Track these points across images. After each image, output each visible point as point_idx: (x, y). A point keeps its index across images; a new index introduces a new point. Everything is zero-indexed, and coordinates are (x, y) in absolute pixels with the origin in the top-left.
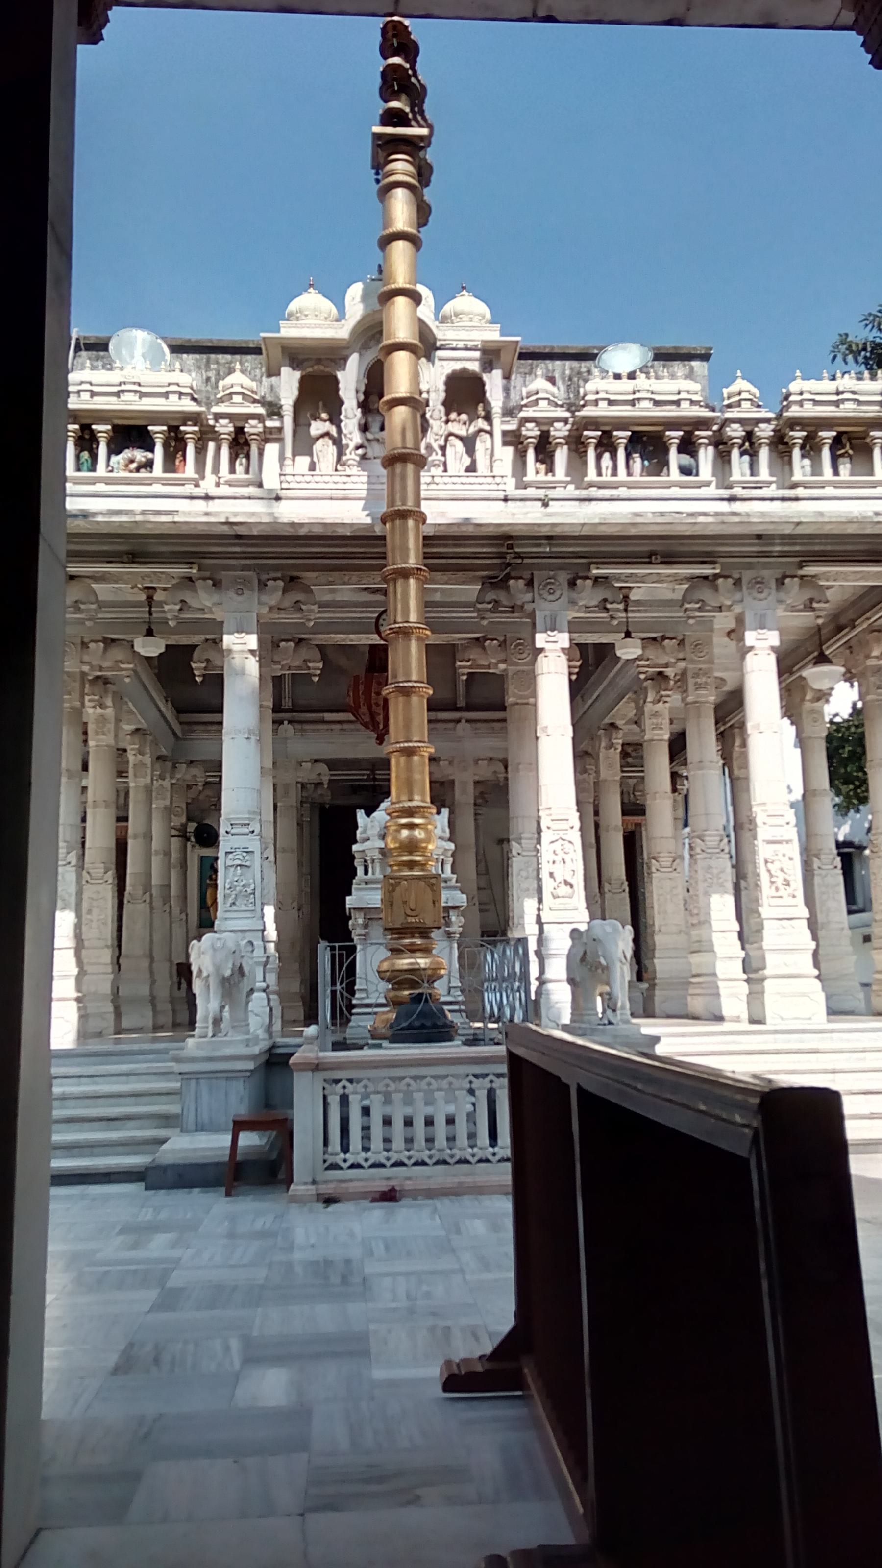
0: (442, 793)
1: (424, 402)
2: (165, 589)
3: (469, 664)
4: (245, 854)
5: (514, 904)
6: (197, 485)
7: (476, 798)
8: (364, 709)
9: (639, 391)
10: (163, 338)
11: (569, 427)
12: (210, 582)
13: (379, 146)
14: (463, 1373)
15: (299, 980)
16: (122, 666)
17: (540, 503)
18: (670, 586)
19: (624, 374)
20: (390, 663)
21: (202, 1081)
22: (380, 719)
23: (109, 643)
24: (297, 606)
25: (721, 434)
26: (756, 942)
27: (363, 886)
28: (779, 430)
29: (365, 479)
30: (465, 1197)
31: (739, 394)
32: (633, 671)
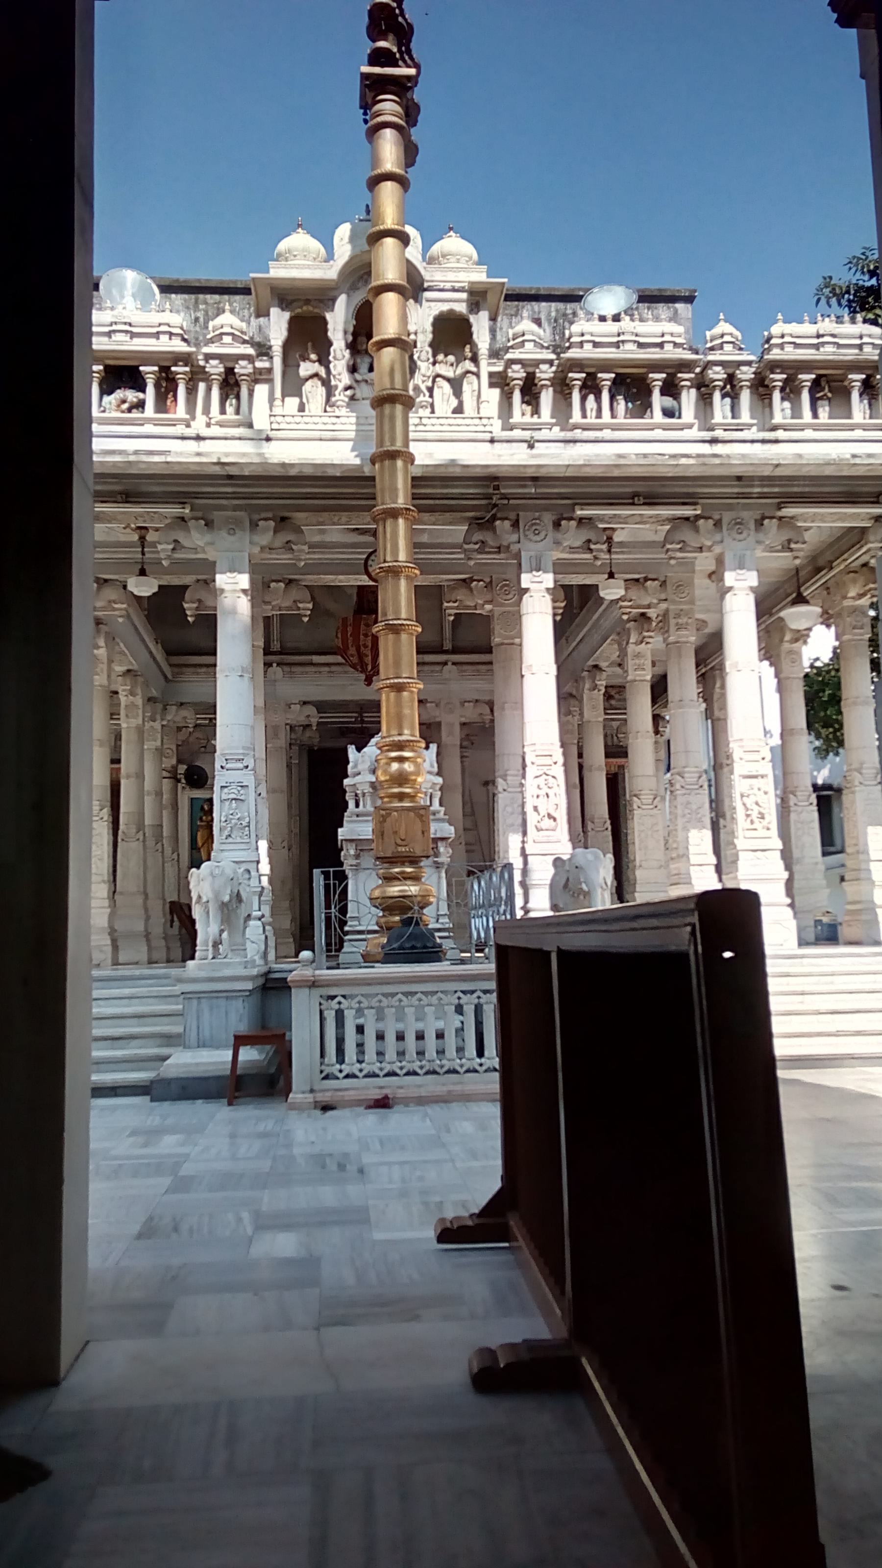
0: (429, 731)
1: (412, 344)
2: (157, 530)
3: (456, 604)
4: (239, 788)
5: (500, 839)
6: (188, 426)
7: (462, 740)
8: (352, 650)
9: (623, 333)
10: (151, 278)
11: (554, 369)
12: (203, 522)
13: (366, 86)
14: (455, 1227)
15: (290, 917)
16: (116, 606)
17: (525, 445)
18: (653, 527)
19: (609, 316)
20: (376, 602)
21: (203, 1001)
22: (368, 660)
23: (103, 583)
24: (288, 546)
25: (703, 376)
26: (731, 873)
27: (355, 818)
28: (760, 373)
29: (354, 420)
30: (454, 1104)
31: (722, 336)
32: (616, 613)
